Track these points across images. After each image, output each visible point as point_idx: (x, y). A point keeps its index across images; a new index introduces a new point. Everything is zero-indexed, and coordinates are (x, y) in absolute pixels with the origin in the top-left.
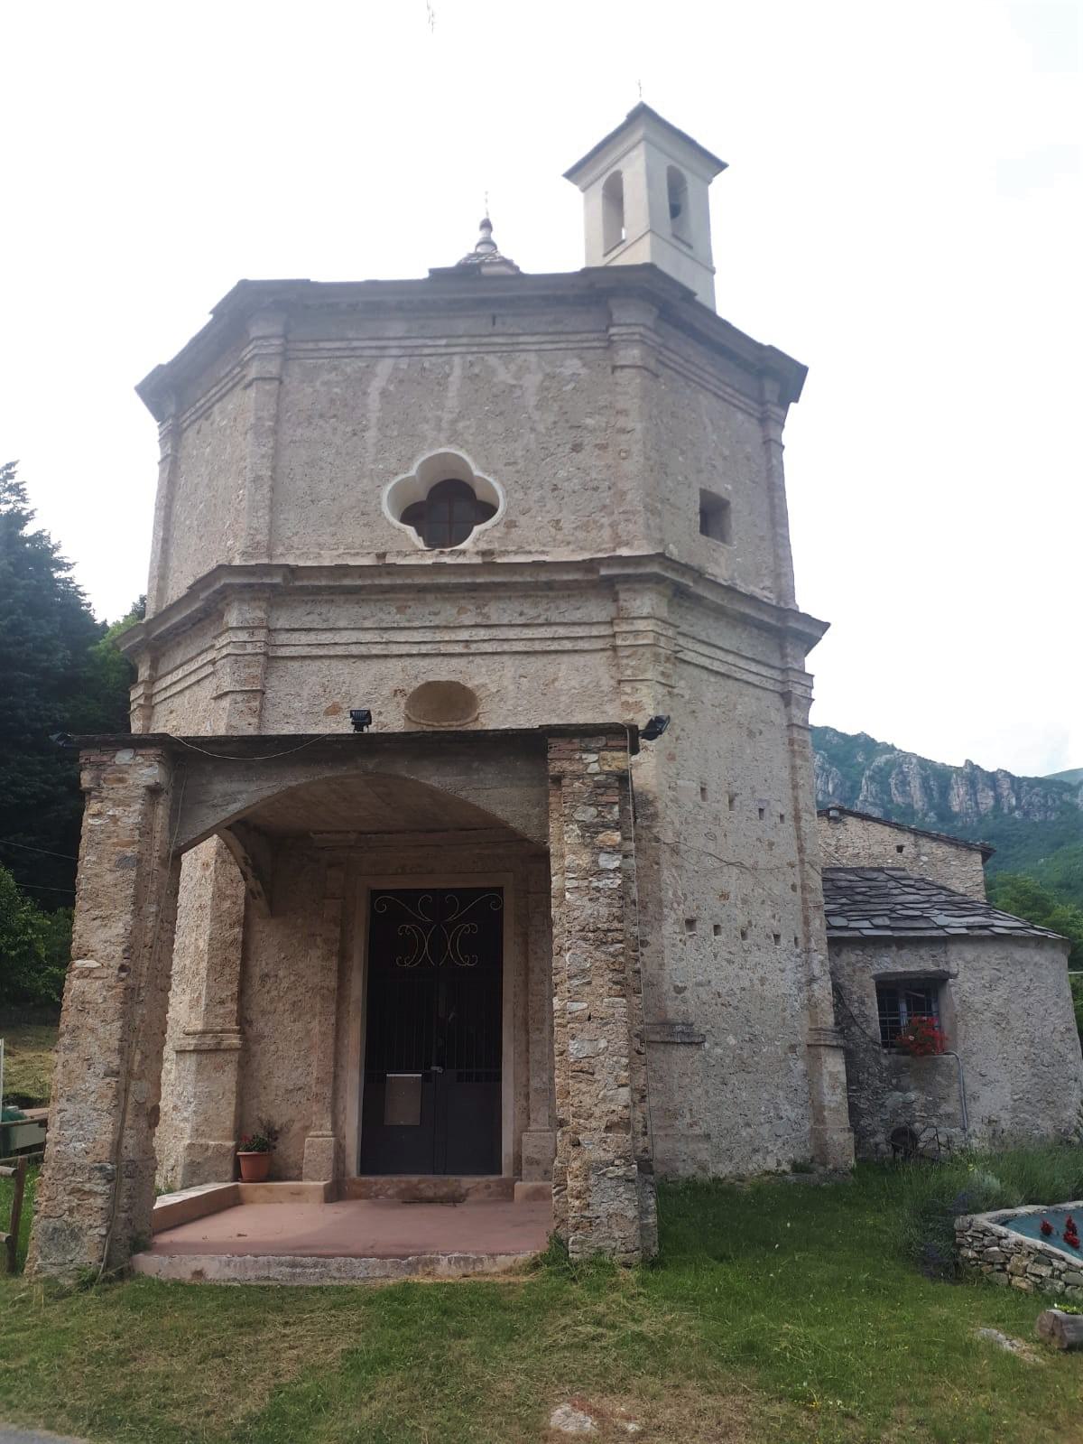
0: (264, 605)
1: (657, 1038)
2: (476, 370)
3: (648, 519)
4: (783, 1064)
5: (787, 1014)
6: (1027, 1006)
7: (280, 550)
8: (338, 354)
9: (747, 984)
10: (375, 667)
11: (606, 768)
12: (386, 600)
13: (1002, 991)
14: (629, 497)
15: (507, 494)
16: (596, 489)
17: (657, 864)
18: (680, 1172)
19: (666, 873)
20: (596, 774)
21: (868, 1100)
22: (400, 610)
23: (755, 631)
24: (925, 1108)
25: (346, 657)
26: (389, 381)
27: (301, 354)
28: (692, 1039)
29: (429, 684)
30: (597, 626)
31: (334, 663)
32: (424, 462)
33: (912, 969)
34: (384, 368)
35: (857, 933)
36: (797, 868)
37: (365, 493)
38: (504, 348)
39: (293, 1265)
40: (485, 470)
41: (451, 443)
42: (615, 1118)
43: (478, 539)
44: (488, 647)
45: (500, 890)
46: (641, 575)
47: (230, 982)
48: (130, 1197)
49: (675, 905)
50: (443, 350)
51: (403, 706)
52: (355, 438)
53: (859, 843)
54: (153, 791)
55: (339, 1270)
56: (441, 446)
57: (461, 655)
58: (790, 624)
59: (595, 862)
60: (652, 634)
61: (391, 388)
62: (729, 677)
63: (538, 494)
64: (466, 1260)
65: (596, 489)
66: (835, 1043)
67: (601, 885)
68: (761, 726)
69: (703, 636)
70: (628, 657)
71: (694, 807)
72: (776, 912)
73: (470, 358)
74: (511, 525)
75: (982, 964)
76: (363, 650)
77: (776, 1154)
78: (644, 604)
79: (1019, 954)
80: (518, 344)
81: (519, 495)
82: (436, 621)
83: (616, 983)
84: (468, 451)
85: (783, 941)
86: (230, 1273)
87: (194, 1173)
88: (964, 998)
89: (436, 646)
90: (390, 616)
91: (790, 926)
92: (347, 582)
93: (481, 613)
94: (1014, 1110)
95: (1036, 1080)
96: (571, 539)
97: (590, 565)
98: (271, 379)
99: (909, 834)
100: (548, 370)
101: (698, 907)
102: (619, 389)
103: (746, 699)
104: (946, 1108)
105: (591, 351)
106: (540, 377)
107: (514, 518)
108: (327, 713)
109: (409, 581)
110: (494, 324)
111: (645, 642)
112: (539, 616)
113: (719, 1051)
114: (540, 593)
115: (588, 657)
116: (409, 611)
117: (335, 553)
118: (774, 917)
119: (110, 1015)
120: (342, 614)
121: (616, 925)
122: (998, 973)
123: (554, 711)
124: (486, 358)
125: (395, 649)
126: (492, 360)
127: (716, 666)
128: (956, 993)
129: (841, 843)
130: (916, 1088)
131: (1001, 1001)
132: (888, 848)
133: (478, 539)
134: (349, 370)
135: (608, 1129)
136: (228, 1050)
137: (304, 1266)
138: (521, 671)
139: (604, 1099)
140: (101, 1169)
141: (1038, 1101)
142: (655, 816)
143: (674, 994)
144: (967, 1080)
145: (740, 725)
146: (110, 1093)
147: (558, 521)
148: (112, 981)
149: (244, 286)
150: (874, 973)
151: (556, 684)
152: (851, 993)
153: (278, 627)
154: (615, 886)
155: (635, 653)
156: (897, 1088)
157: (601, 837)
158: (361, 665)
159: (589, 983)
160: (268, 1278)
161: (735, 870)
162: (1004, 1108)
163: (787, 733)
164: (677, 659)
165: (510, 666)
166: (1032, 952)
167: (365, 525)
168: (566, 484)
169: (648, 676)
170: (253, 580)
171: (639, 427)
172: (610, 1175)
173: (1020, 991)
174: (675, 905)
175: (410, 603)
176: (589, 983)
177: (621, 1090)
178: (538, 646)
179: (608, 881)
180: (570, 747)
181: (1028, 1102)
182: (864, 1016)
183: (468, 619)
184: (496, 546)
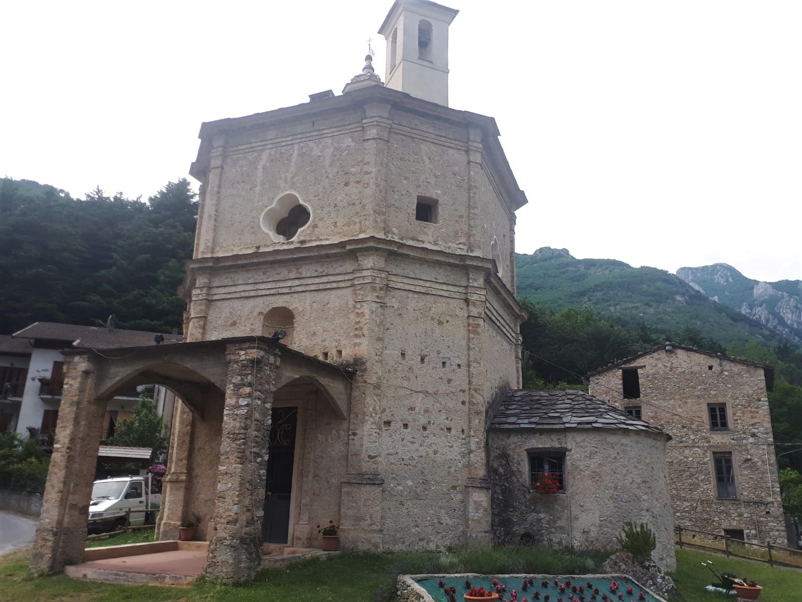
0: (208, 276)
1: (355, 481)
2: (304, 150)
3: (376, 218)
4: (446, 496)
5: (452, 470)
6: (614, 468)
7: (218, 249)
8: (247, 151)
9: (424, 454)
10: (252, 302)
11: (248, 357)
12: (259, 269)
13: (597, 459)
14: (367, 207)
15: (314, 211)
16: (354, 204)
17: (364, 394)
18: (360, 548)
19: (368, 399)
20: (244, 360)
21: (518, 517)
22: (264, 273)
23: (448, 268)
24: (548, 523)
25: (240, 298)
26: (267, 161)
27: (231, 153)
29: (274, 309)
30: (348, 275)
31: (236, 301)
32: (279, 200)
33: (547, 446)
34: (265, 155)
35: (517, 426)
36: (467, 392)
37: (254, 218)
38: (317, 137)
39: (116, 575)
40: (305, 201)
41: (291, 188)
42: (230, 518)
43: (300, 235)
44: (299, 289)
45: (296, 408)
46: (365, 248)
47: (185, 451)
48: (64, 542)
49: (374, 415)
50: (291, 142)
51: (262, 320)
52: (251, 191)
53: (684, 365)
54: (86, 373)
55: (131, 578)
56: (287, 191)
57: (288, 293)
58: (467, 263)
59: (237, 402)
60: (370, 278)
61: (267, 165)
62: (427, 294)
63: (327, 209)
64: (176, 577)
65: (354, 204)
66: (479, 486)
67: (238, 412)
68: (448, 318)
70: (360, 290)
72: (449, 416)
73: (302, 144)
74: (315, 226)
76: (247, 294)
77: (436, 542)
78: (369, 262)
79: (612, 439)
80: (323, 134)
81: (319, 211)
82: (279, 277)
83: (239, 458)
84: (298, 192)
85: (453, 432)
86: (95, 576)
87: (166, 535)
89: (277, 290)
90: (260, 277)
91: (459, 423)
92: (240, 262)
93: (298, 272)
94: (600, 526)
96: (341, 231)
97: (342, 244)
98: (218, 167)
99: (716, 359)
100: (336, 145)
101: (392, 415)
102: (366, 151)
103: (439, 305)
104: (560, 523)
105: (356, 133)
106: (332, 150)
107: (316, 223)
108: (231, 325)
109: (265, 260)
110: (313, 125)
111: (368, 281)
112: (323, 272)
113: (400, 488)
114: (324, 260)
115: (344, 290)
116: (268, 273)
117: (239, 248)
118: (447, 419)
119: (62, 467)
120: (240, 278)
121: (242, 431)
122: (596, 449)
123: (326, 319)
124: (309, 143)
125: (260, 293)
126: (312, 144)
127: (418, 289)
128: (570, 460)
129: (674, 365)
130: (544, 512)
132: (703, 367)
133: (300, 235)
134: (250, 158)
135: (228, 523)
136: (181, 481)
137: (120, 576)
138: (313, 300)
139: (227, 510)
140: (52, 530)
141: (617, 522)
142: (365, 370)
143: (367, 459)
145: (433, 319)
146: (58, 499)
147: (336, 223)
148: (64, 453)
150: (526, 448)
151: (329, 305)
152: (514, 459)
153: (214, 286)
154: (244, 413)
155: (362, 287)
156: (533, 511)
157: (241, 390)
158: (246, 301)
159: (228, 458)
160: (107, 580)
161: (421, 396)
162: (593, 525)
163: (466, 320)
164: (388, 288)
165: (309, 297)
167: (252, 233)
168: (340, 203)
169: (369, 299)
170: (201, 265)
171: (374, 170)
172: (224, 544)
174: (374, 415)
175: (268, 270)
176: (228, 458)
177: (235, 506)
178: (321, 287)
179: (241, 411)
180: (235, 348)
181: (611, 522)
182: (520, 471)
183: (292, 276)
184: (307, 238)
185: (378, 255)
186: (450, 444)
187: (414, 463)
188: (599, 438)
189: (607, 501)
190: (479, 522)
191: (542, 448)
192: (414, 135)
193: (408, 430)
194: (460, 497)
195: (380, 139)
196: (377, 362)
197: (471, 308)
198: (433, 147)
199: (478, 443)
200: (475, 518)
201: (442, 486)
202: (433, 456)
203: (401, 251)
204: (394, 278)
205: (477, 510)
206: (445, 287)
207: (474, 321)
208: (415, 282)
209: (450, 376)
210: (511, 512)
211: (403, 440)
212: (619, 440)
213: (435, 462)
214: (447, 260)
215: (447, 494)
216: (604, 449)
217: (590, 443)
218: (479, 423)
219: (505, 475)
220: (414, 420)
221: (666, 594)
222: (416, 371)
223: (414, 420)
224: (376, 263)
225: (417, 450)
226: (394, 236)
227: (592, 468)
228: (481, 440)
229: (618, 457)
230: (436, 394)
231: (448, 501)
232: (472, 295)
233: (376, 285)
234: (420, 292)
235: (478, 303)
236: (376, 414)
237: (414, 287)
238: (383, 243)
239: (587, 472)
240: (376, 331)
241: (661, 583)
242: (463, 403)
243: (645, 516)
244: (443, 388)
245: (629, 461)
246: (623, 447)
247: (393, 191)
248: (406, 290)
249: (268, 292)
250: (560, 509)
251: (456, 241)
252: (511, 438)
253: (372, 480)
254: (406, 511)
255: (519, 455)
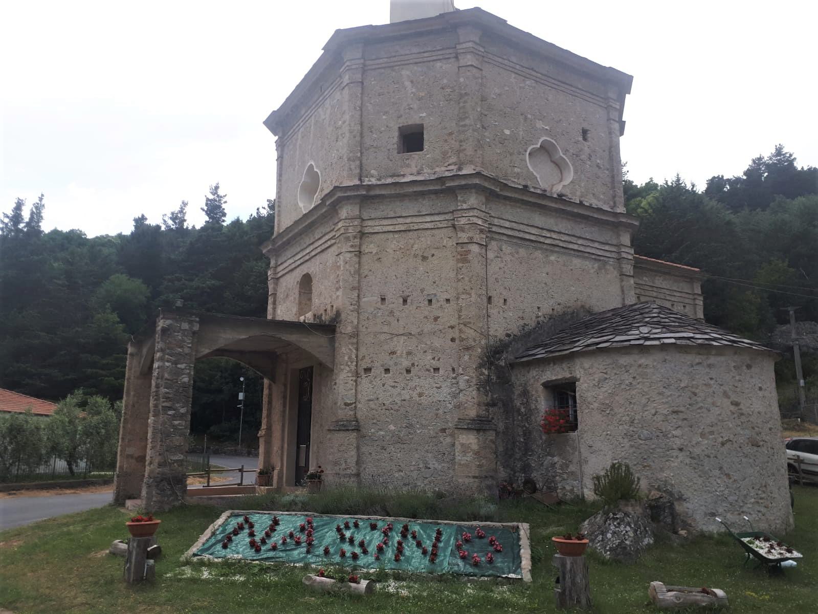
4: (434, 440)
5: (441, 412)
9: (408, 397)
13: (607, 387)
19: (344, 348)
21: (535, 461)
23: (433, 196)
28: (347, 428)
29: (304, 275)
49: (349, 363)
58: (447, 185)
62: (409, 231)
66: (466, 427)
69: (392, 214)
71: (375, 310)
75: (595, 370)
79: (624, 360)
88: (582, 394)
95: (634, 449)
104: (572, 468)
118: (434, 359)
122: (606, 376)
127: (397, 228)
131: (606, 394)
141: (635, 465)
144: (582, 450)
145: (415, 256)
149: (338, 32)
150: (543, 381)
156: (549, 454)
166: (636, 357)
173: (623, 387)
185: (351, 204)
186: (438, 386)
187: (397, 407)
188: (609, 361)
189: (621, 440)
190: (467, 466)
191: (556, 380)
192: (392, 64)
193: (390, 375)
194: (450, 441)
195: (351, 83)
196: (352, 311)
197: (460, 234)
198: (416, 68)
199: (468, 381)
200: (462, 462)
201: (430, 430)
202: (418, 399)
203: (372, 193)
204: (370, 223)
205: (464, 453)
206: (428, 219)
207: (462, 248)
208: (394, 221)
209: (437, 313)
210: (530, 455)
211: (384, 385)
212: (635, 361)
213: (421, 404)
214: (426, 188)
215: (435, 437)
216: (616, 374)
217: (599, 369)
218: (470, 359)
219: (526, 415)
220: (396, 364)
221: (608, 553)
222: (397, 314)
223: (396, 364)
224: (349, 212)
225: (400, 394)
226: (371, 179)
227: (601, 399)
228: (472, 378)
229: (634, 383)
230: (420, 334)
231: (436, 445)
232: (459, 219)
233: (349, 235)
234: (400, 231)
235: (467, 226)
236: (352, 362)
237: (392, 227)
238: (350, 190)
239: (596, 405)
240: (350, 281)
241: (610, 539)
242: (453, 340)
243: (677, 457)
244: (428, 327)
245: (651, 387)
246: (640, 370)
247: (371, 132)
248: (385, 232)
249: (302, 261)
250: (571, 451)
251: (444, 163)
252: (531, 373)
253: (345, 426)
254: (389, 455)
255: (537, 391)
